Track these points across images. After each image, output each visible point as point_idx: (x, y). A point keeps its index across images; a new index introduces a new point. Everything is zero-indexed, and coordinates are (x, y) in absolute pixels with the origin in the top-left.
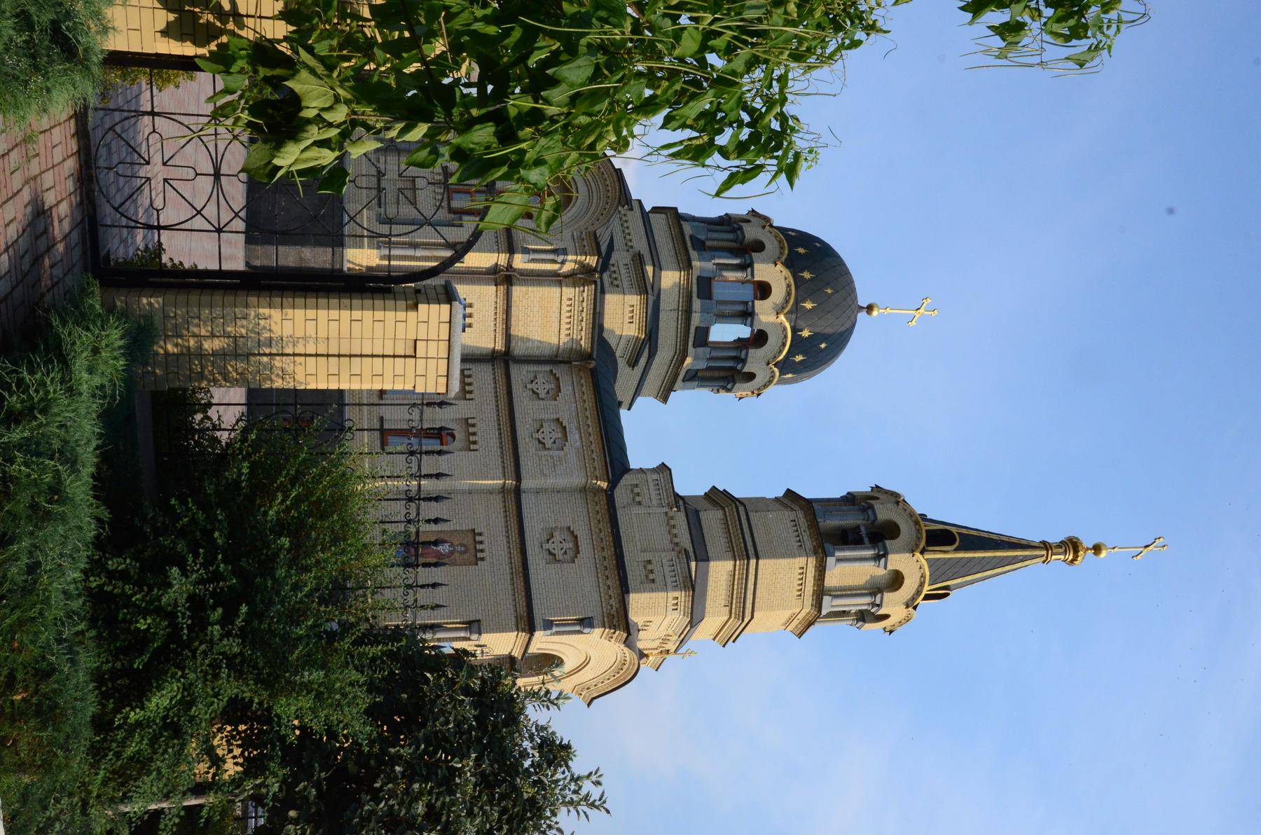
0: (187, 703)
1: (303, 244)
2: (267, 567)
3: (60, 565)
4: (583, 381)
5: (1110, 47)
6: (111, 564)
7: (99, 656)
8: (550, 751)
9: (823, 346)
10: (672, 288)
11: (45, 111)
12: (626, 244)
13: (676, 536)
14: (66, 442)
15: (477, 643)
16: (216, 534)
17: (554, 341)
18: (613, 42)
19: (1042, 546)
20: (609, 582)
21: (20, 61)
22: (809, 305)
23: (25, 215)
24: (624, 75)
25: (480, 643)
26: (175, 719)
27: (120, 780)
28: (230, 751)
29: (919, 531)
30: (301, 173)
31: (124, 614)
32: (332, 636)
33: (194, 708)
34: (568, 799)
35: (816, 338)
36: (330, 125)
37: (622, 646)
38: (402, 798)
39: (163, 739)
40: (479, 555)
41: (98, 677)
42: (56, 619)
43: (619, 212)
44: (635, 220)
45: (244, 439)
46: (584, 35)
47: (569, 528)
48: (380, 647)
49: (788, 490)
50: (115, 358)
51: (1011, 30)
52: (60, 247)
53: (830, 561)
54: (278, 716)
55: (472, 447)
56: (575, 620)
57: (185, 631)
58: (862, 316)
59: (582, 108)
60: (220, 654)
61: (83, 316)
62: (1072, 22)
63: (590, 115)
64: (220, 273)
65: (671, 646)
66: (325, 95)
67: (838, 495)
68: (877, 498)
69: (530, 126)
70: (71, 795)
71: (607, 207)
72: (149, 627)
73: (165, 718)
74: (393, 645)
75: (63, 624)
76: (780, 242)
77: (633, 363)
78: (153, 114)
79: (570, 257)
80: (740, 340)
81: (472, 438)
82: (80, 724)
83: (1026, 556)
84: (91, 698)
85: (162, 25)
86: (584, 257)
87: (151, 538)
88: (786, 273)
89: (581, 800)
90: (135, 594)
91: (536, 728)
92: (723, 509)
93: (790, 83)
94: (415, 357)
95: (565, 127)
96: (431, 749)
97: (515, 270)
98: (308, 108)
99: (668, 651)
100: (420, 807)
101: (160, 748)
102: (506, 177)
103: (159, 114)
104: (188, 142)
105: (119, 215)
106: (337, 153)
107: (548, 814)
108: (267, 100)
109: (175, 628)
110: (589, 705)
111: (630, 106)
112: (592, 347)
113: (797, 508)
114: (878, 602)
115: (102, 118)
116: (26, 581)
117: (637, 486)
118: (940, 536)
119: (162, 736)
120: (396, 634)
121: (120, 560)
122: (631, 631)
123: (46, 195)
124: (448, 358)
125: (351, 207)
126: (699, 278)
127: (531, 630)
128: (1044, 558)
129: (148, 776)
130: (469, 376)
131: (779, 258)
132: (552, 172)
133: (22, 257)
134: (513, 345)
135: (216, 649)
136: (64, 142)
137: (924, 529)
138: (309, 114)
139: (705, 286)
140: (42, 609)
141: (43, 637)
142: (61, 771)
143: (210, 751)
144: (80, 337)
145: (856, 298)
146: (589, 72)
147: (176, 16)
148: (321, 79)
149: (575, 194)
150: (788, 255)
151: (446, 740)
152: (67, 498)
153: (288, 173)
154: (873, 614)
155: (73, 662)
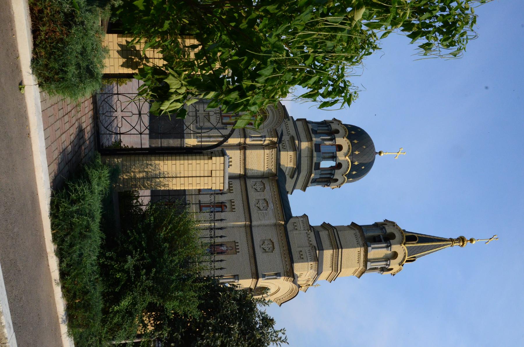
0: (134, 304)
1: (169, 138)
2: (161, 254)
3: (89, 254)
4: (273, 184)
5: (465, 49)
6: (107, 254)
7: (103, 287)
8: (266, 321)
9: (363, 168)
10: (305, 149)
11: (83, 95)
12: (288, 133)
13: (310, 241)
14: (90, 210)
15: (237, 283)
16: (143, 243)
17: (262, 170)
18: (279, 60)
19: (450, 240)
20: (286, 259)
21: (76, 79)
22: (357, 153)
23: (76, 132)
24: (284, 71)
25: (239, 283)
26: (130, 310)
27: (112, 332)
28: (150, 322)
29: (403, 236)
30: (170, 112)
31: (111, 272)
32: (184, 280)
33: (137, 306)
34: (273, 339)
35: (360, 165)
36: (180, 94)
37: (292, 283)
38: (212, 339)
39: (126, 317)
40: (237, 250)
41: (103, 294)
42: (89, 273)
43: (285, 121)
44: (290, 124)
45: (151, 208)
46: (270, 57)
47: (270, 239)
48: (202, 284)
49: (352, 223)
50: (106, 180)
51: (427, 47)
52: (88, 142)
53: (369, 248)
54: (166, 308)
55: (233, 210)
56: (274, 274)
57: (133, 278)
58: (377, 156)
59: (269, 83)
60: (145, 286)
61: (95, 166)
62: (450, 41)
63: (272, 86)
64: (142, 149)
65: (310, 283)
66: (178, 84)
67: (371, 224)
68: (386, 224)
69: (251, 91)
70: (96, 336)
71: (280, 119)
72: (120, 277)
73: (126, 309)
74: (207, 283)
75: (91, 275)
76: (345, 129)
77: (292, 177)
78: (118, 94)
79: (267, 139)
80: (332, 167)
81: (233, 207)
82: (98, 311)
83: (444, 244)
84: (101, 302)
85: (121, 63)
86: (272, 138)
87: (120, 245)
88: (348, 141)
89: (278, 339)
90: (115, 265)
91: (260, 313)
92: (328, 230)
93: (345, 70)
94: (212, 176)
95: (263, 91)
96: (222, 321)
97: (247, 144)
98: (172, 88)
99: (309, 285)
100: (219, 342)
101: (125, 320)
102: (243, 110)
103: (120, 94)
104: (130, 103)
105: (106, 130)
106: (182, 104)
107: (266, 345)
108: (158, 87)
109: (129, 277)
110: (280, 306)
111: (287, 82)
112: (276, 172)
113: (356, 229)
114: (388, 264)
115: (101, 97)
116: (78, 260)
117: (295, 223)
118: (411, 238)
119: (126, 316)
120: (208, 279)
121: (110, 253)
122: (295, 277)
123: (83, 124)
124: (224, 177)
125: (187, 124)
126: (315, 144)
127: (257, 278)
128: (451, 245)
129: (122, 330)
130: (231, 184)
131: (345, 136)
132: (259, 107)
133: (75, 146)
134: (247, 172)
135: (144, 284)
136: (88, 106)
137: (405, 235)
138: (172, 91)
139: (318, 147)
140: (84, 270)
141: (85, 280)
142: (92, 328)
143: (142, 322)
144: (94, 173)
145: (375, 149)
146: (271, 71)
147: (126, 59)
148: (177, 78)
149: (268, 115)
150: (348, 134)
151: (227, 317)
152: (91, 230)
153: (165, 112)
154: (387, 268)
155: (95, 289)
